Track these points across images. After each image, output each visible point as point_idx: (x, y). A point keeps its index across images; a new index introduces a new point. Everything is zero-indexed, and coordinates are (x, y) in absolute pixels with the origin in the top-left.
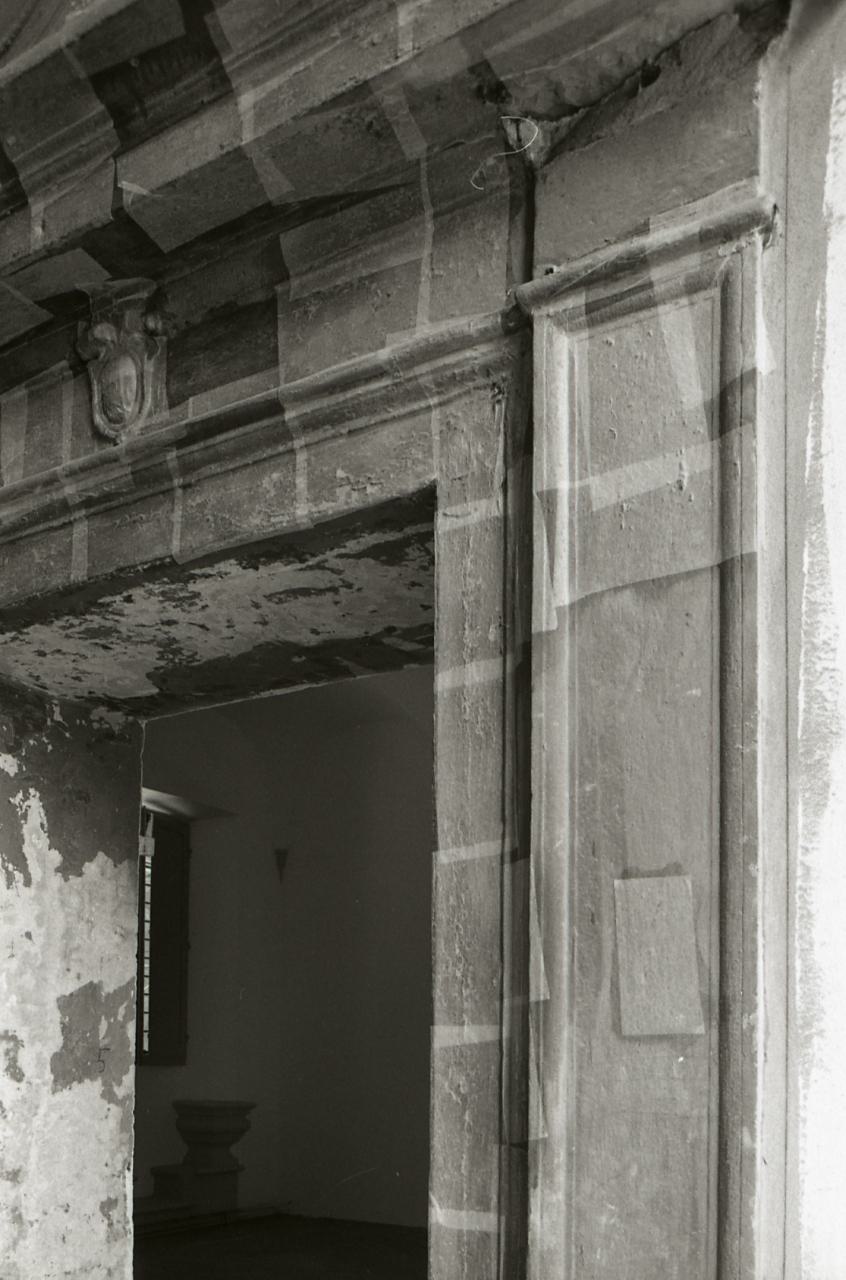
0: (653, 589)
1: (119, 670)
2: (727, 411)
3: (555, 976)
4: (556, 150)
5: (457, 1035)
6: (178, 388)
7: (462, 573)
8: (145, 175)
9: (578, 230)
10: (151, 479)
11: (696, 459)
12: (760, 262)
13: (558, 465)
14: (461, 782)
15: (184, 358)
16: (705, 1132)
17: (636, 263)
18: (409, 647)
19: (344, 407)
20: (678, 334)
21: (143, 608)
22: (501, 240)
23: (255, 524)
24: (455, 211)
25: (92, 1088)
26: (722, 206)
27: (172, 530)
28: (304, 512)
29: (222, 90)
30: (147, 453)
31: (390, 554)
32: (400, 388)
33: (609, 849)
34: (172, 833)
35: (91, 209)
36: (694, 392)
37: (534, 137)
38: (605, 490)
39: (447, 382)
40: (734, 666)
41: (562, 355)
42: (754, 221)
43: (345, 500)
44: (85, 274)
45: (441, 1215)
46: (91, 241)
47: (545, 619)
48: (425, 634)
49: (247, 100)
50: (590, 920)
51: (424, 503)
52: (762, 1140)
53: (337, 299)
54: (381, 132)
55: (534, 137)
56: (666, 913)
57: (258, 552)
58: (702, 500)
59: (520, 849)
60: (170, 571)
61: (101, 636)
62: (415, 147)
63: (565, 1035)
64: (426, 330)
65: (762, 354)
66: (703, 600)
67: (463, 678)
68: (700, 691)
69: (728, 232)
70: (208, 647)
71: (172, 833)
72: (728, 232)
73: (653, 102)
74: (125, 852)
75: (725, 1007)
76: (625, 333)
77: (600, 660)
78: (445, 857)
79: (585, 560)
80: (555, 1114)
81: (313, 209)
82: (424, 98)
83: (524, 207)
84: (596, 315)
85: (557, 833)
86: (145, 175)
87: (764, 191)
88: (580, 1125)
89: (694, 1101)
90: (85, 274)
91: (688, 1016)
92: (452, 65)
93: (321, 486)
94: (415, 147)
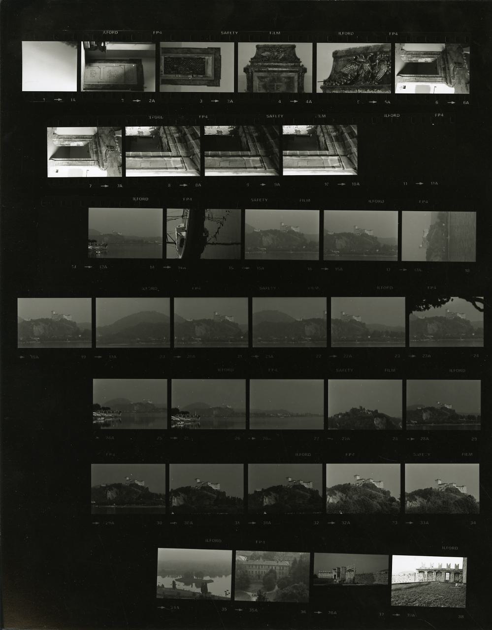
0: (323, 163)
1: (161, 134)
2: (176, 168)
3: (301, 158)
4: (348, 158)
5: (298, 152)
6: (177, 138)
7: (246, 153)
8: (346, 134)
9: (186, 160)
10: (329, 135)
11: (173, 166)
12: (184, 170)
13: (330, 158)
14: (155, 154)
15: (336, 137)
16: (215, 167)
17: (341, 162)
18: (320, 149)
19: (176, 147)
20: (180, 165)
21: (165, 136)
22: (343, 154)
23: (169, 142)
24: (187, 153)
25: (138, 133)
26: (187, 168)
27: (326, 136)
28: (327, 143)
29: (351, 139)
30: (252, 135)
31: (168, 149)
32: (177, 150)
33: (151, 162)
34: (309, 136)
35: (187, 133)
36: (177, 166)
37: (191, 157)
38: (251, 161)
39: (257, 152)
40: (148, 171)
41: (179, 159)
42: (266, 169)
43: (171, 147)
44: (340, 131)
45: (131, 153)
46: (342, 131)
47: (243, 158)
48: (163, 151)
49: (193, 141)
50: (147, 161)
51: (171, 151)
52: (135, 170)
53: (339, 145)
54: (348, 147)
55: (270, 157)
56: (81, 164)
57: (168, 142)
58: (250, 166)
59: (309, 156)
60: (324, 136)
61: (163, 133)
62: (191, 151)
63: (141, 159)
64: (180, 151)
65: (336, 169)
66: (244, 166)
67: (161, 154)
68: (317, 166)
69: (265, 168)
70: (162, 139)
71: (309, 136)
72: (265, 168)
73: (193, 164)
74: (308, 134)
75: (222, 168)
76: (259, 162)
77: (319, 160)
78: (230, 152)
79: (247, 160)
80: (294, 158)
81: (344, 143)
82: (194, 152)
83: (187, 157)
84: (260, 160)
85: (310, 158)
86: (346, 134)
87: (267, 170)
88: (293, 159)
89: (216, 166)
90: (340, 131)
91: (142, 167)
92: (195, 153)
93: (172, 145)
94: (348, 150)
